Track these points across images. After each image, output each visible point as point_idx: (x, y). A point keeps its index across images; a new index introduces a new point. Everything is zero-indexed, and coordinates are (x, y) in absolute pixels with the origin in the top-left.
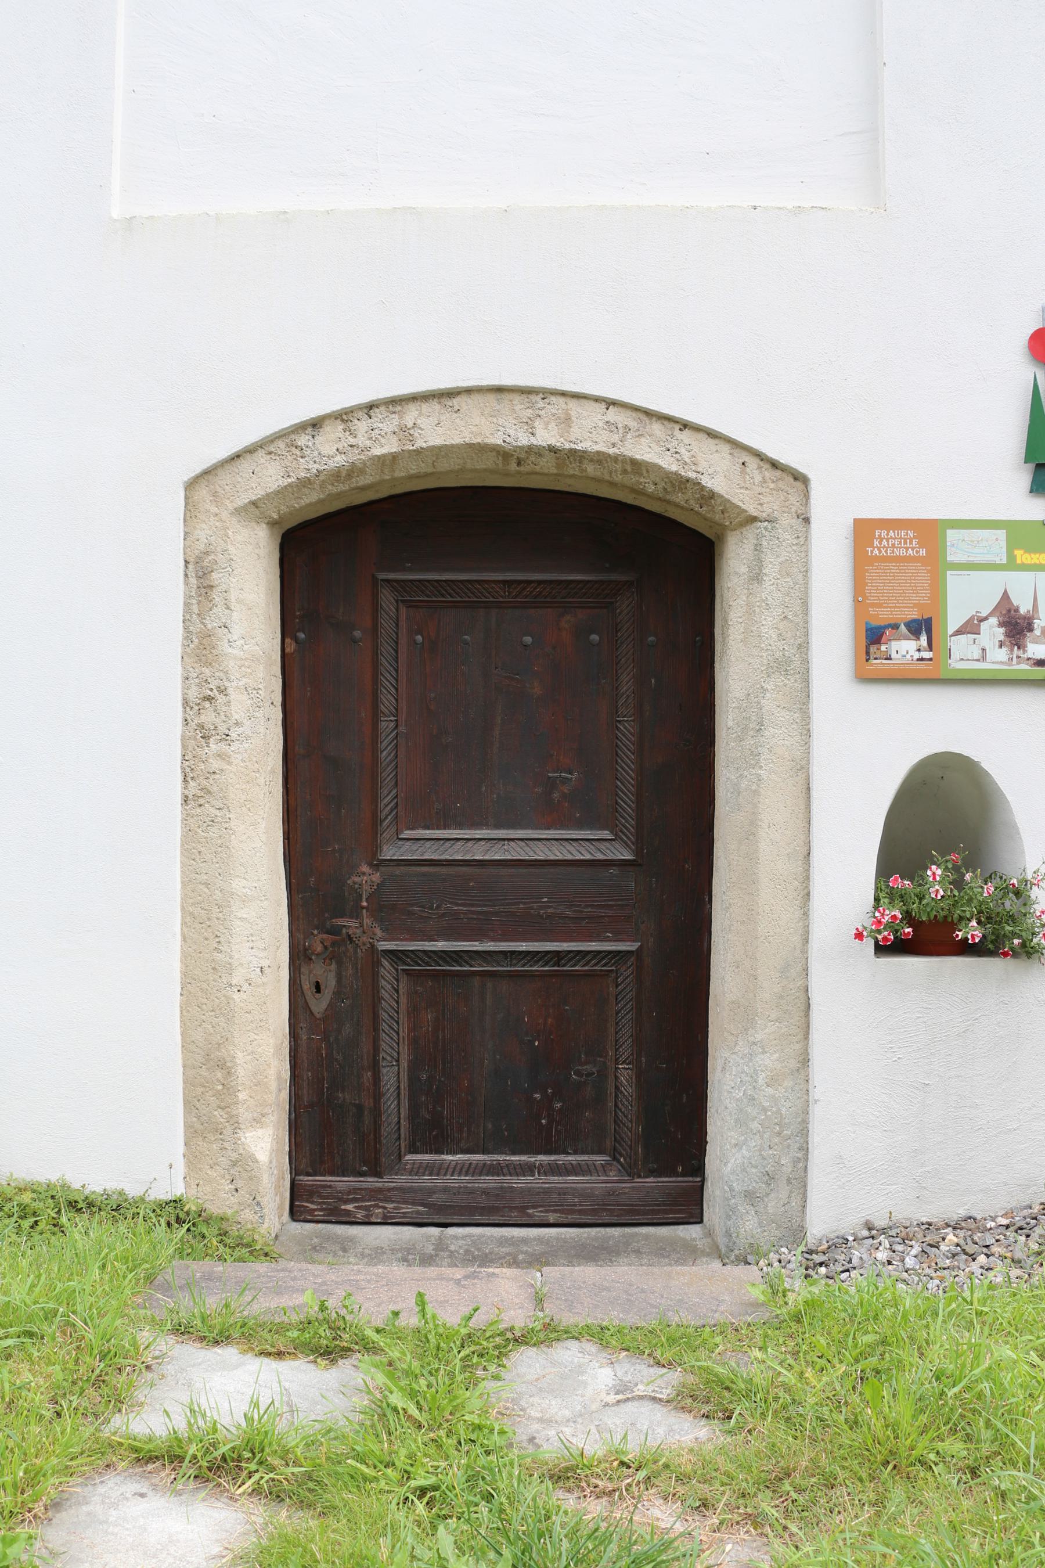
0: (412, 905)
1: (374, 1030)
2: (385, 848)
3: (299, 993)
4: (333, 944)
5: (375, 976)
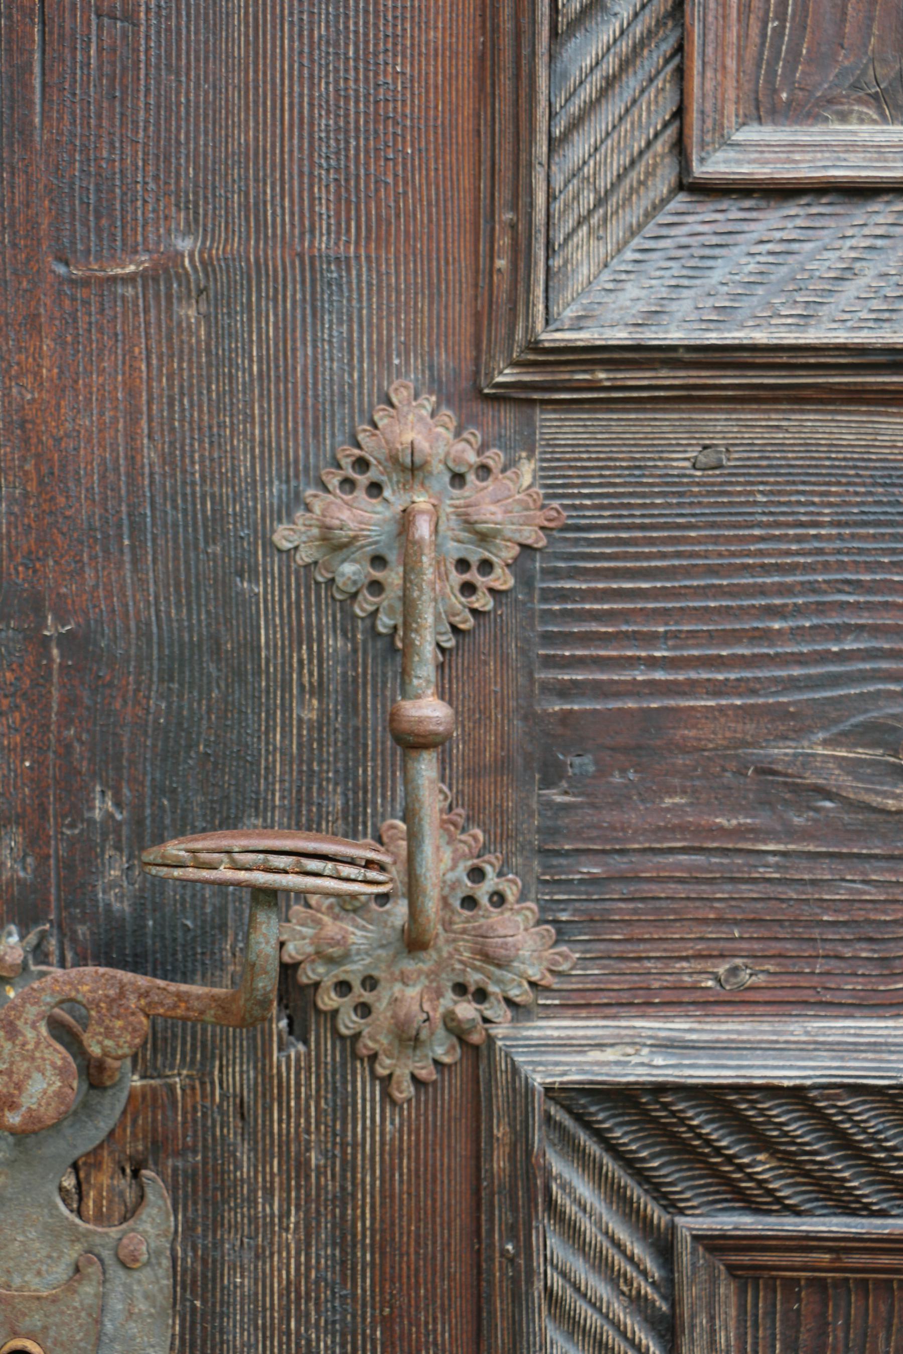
0: (793, 723)
2: (583, 258)
4: (161, 1041)
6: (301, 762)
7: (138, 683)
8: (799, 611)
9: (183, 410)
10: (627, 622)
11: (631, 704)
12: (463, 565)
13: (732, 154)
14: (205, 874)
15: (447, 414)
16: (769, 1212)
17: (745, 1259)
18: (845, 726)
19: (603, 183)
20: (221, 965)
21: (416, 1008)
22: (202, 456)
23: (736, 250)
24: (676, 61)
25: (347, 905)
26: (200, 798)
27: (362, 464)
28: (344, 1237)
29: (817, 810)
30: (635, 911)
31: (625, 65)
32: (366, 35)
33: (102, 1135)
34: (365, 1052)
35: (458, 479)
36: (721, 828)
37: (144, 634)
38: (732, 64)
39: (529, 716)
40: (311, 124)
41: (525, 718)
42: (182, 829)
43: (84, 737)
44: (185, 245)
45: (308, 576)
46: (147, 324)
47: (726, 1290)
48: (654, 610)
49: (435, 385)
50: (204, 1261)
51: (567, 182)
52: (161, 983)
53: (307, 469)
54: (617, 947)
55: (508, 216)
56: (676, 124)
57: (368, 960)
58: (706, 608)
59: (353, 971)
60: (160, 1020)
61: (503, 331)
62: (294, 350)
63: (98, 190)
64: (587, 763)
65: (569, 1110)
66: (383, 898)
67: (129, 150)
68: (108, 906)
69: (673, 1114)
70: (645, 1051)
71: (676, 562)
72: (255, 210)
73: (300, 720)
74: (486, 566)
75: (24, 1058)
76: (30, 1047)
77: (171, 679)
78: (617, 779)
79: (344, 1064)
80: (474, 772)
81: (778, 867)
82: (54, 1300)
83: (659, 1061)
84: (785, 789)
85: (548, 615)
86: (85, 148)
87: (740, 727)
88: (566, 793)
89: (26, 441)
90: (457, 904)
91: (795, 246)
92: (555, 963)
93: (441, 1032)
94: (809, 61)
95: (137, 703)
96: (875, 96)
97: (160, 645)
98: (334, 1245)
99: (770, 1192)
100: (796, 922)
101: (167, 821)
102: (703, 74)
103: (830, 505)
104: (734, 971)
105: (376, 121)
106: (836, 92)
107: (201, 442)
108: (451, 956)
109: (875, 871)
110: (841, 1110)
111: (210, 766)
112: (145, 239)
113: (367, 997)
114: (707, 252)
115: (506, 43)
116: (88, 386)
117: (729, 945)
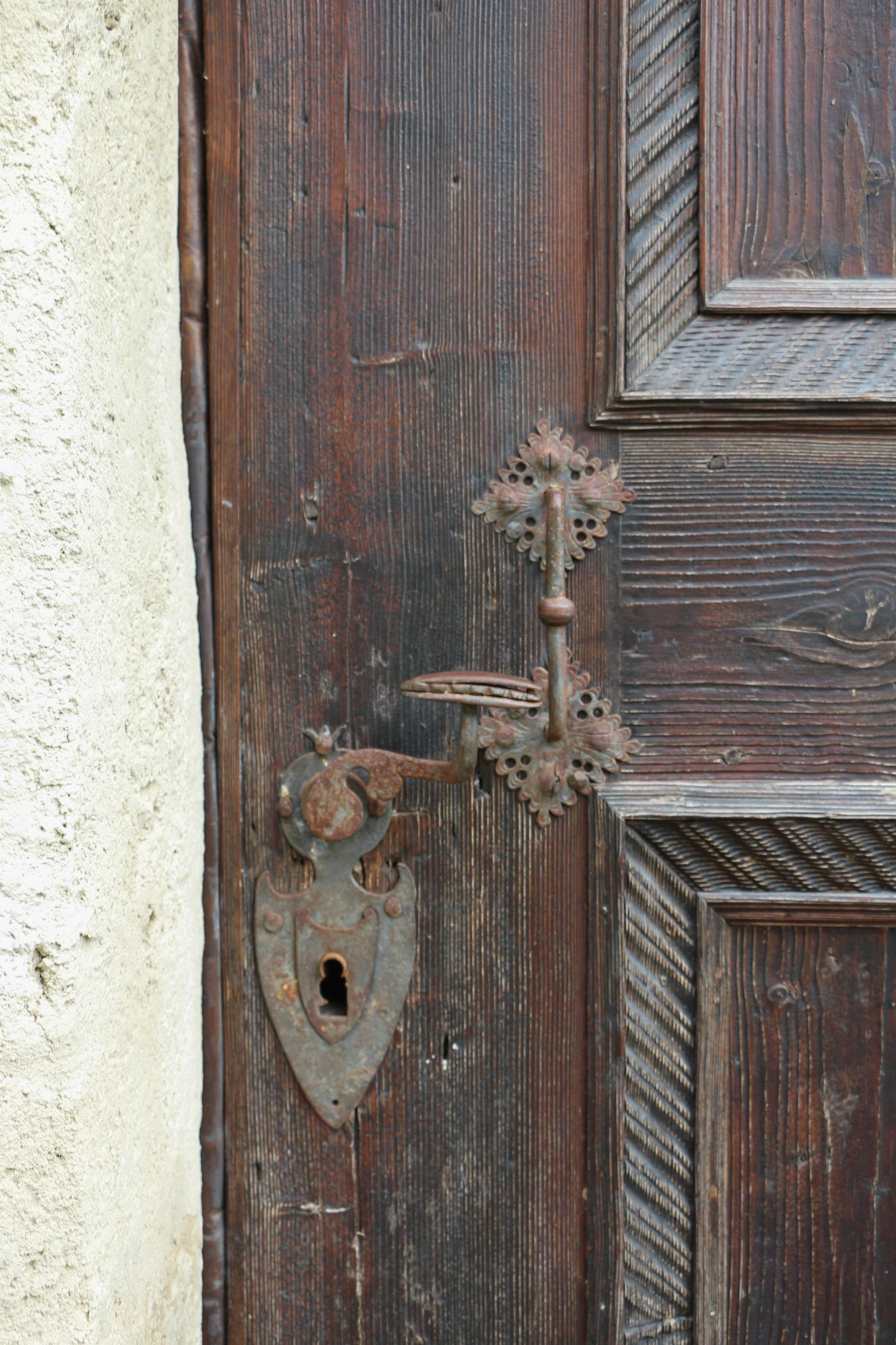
0: (767, 612)
1: (587, 1179)
2: (645, 351)
3: (249, 1014)
4: (410, 790)
5: (597, 939)
6: (487, 634)
7: (396, 590)
8: (768, 549)
9: (421, 437)
10: (671, 555)
11: (674, 602)
12: (578, 523)
13: (727, 295)
14: (437, 696)
15: (569, 438)
16: (750, 890)
17: (736, 915)
18: (795, 614)
19: (656, 310)
20: (442, 749)
21: (552, 774)
22: (432, 464)
23: (730, 347)
24: (695, 245)
25: (513, 714)
26: (430, 655)
27: (521, 466)
28: (511, 902)
29: (780, 662)
30: (676, 720)
31: (667, 246)
32: (523, 232)
33: (377, 843)
34: (523, 799)
35: (575, 474)
36: (725, 673)
37: (400, 562)
38: (726, 246)
39: (616, 608)
40: (493, 280)
41: (614, 610)
42: (419, 673)
43: (366, 620)
44: (423, 346)
45: (492, 529)
46: (402, 390)
47: (726, 933)
48: (687, 548)
49: (562, 421)
50: (433, 914)
51: (636, 310)
52: (410, 758)
53: (490, 469)
54: (666, 740)
55: (603, 328)
56: (695, 279)
57: (525, 747)
58: (717, 548)
59: (516, 753)
60: (408, 780)
61: (601, 392)
62: (483, 403)
63: (376, 317)
64: (649, 635)
65: (638, 832)
66: (533, 711)
67: (392, 296)
68: (379, 715)
69: (698, 834)
70: (682, 799)
71: (699, 521)
72: (461, 328)
73: (486, 611)
74: (592, 524)
75: (334, 799)
76: (338, 793)
77: (414, 588)
78: (666, 644)
79: (511, 805)
80: (585, 640)
81: (757, 694)
82: (351, 933)
83: (690, 804)
84: (761, 650)
85: (627, 551)
86: (369, 296)
87: (736, 615)
88: (637, 652)
89: (335, 455)
90: (575, 715)
91: (764, 345)
92: (631, 749)
93: (566, 788)
94: (769, 245)
95: (395, 601)
96: (806, 264)
97: (408, 568)
98: (505, 907)
99: (752, 879)
100: (767, 726)
101: (412, 668)
102: (710, 251)
103: (785, 489)
104: (732, 754)
105: (529, 278)
106: (784, 262)
107: (431, 455)
108: (572, 745)
109: (812, 697)
110: (793, 832)
111: (436, 637)
112: (401, 343)
113: (524, 767)
114: (715, 348)
115: (601, 235)
116: (369, 425)
117: (730, 739)
